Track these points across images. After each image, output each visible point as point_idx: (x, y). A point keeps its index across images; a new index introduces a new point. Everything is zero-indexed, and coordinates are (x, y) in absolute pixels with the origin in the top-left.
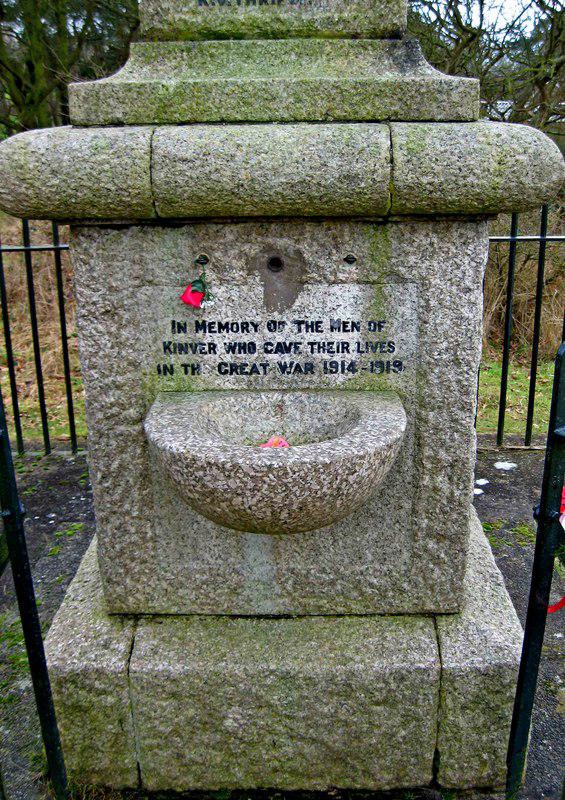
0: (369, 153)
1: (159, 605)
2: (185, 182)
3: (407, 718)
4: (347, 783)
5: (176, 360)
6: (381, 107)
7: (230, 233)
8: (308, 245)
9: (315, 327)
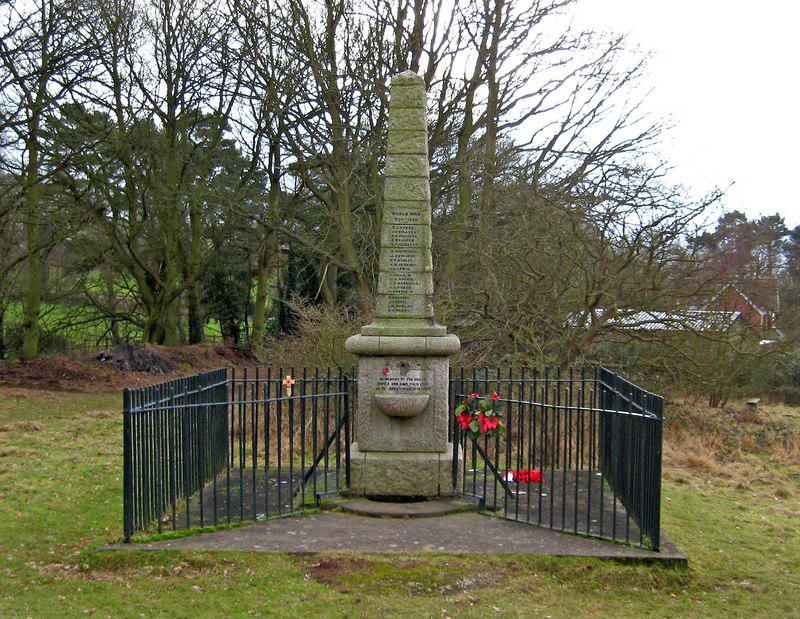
0: (422, 343)
1: (372, 449)
2: (385, 348)
3: (432, 474)
4: (416, 493)
5: (381, 386)
6: (425, 333)
7: (393, 359)
8: (410, 361)
9: (411, 380)
